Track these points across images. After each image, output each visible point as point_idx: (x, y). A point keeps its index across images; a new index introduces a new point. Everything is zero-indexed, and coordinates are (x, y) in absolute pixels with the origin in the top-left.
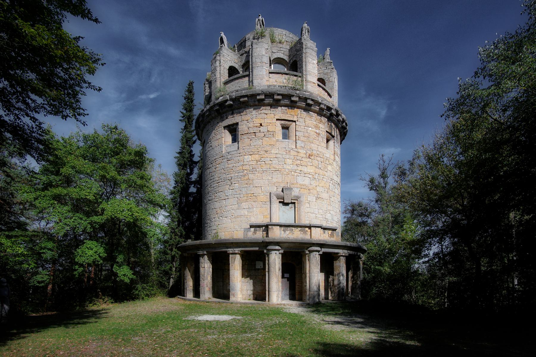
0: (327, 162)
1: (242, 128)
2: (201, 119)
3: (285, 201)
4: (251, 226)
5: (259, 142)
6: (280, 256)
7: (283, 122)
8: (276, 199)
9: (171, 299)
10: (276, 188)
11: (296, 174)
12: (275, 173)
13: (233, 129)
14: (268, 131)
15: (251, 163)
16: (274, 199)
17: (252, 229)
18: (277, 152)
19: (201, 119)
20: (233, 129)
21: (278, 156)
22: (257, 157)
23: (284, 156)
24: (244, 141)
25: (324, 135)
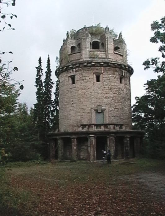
0: (120, 90)
1: (76, 78)
2: (58, 72)
3: (99, 112)
4: (81, 125)
5: (85, 84)
6: (95, 139)
7: (97, 74)
8: (94, 110)
9: (133, 74)
10: (94, 105)
11: (104, 98)
12: (93, 98)
13: (73, 78)
14: (90, 79)
15: (82, 94)
16: (93, 110)
17: (82, 127)
18: (94, 88)
19: (58, 72)
20: (73, 78)
21: (94, 90)
22: (84, 91)
23: (97, 90)
24: (78, 84)
25: (118, 77)
